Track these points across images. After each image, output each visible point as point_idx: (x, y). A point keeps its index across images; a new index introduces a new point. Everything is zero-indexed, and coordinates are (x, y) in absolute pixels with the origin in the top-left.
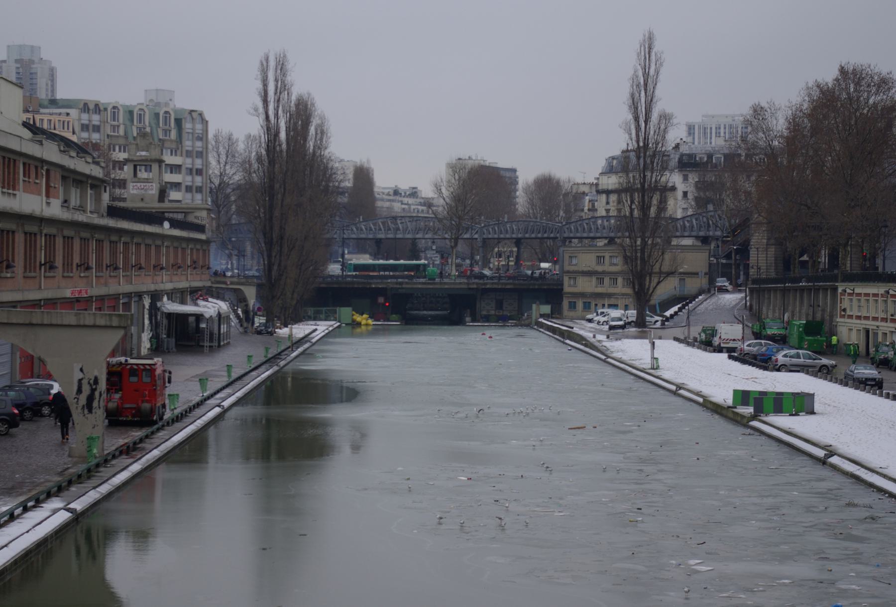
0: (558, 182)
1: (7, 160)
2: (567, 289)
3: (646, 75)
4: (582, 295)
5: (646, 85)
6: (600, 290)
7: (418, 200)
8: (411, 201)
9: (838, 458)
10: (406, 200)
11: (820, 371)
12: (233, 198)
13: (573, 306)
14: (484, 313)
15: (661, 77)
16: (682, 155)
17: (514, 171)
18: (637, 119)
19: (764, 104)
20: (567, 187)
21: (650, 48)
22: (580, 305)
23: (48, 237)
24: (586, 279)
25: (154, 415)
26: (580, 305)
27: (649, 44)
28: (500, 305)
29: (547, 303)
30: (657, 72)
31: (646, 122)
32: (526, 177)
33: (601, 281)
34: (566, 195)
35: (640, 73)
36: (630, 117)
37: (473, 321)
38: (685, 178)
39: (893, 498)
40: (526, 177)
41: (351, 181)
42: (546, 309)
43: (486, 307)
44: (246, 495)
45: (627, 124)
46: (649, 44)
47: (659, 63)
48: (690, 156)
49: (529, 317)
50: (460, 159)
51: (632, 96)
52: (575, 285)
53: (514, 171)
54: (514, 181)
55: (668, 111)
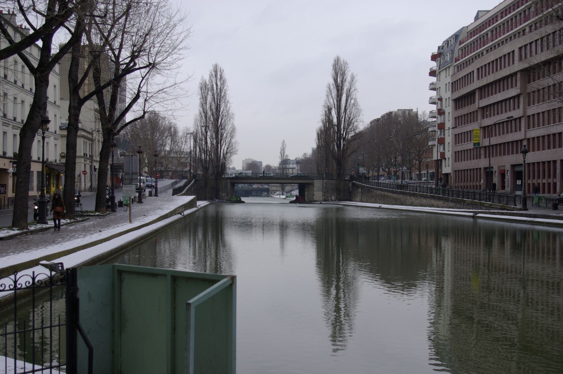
1: (85, 143)
2: (270, 189)
3: (283, 148)
4: (273, 190)
6: (277, 189)
8: (233, 171)
9: (274, 187)
10: (232, 170)
12: (310, 166)
15: (286, 148)
17: (261, 162)
18: (282, 156)
20: (273, 168)
22: (273, 193)
23: (457, 153)
26: (273, 193)
27: (284, 142)
28: (256, 193)
32: (264, 165)
33: (277, 187)
36: (280, 155)
38: (298, 166)
39: (88, 41)
40: (264, 165)
41: (35, 138)
43: (254, 193)
46: (284, 142)
53: (261, 162)
54: (261, 165)
55: (287, 154)
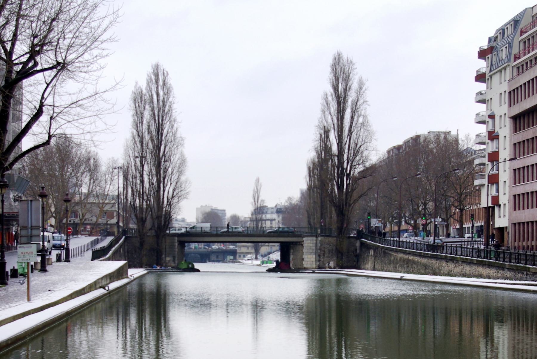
0: (238, 217)
2: (238, 251)
3: (257, 189)
4: (242, 253)
5: (257, 192)
6: (248, 251)
7: (185, 223)
8: (182, 223)
11: (33, 121)
13: (240, 256)
14: (213, 259)
16: (278, 209)
17: (224, 211)
19: (291, 197)
20: (242, 219)
21: (258, 182)
22: (242, 256)
24: (244, 248)
25: (162, 254)
26: (242, 256)
27: (258, 180)
28: (217, 257)
29: (232, 256)
30: (260, 188)
31: (257, 202)
32: (228, 215)
34: (242, 221)
35: (256, 189)
36: (253, 201)
37: (209, 261)
38: (279, 216)
40: (228, 215)
42: (232, 257)
43: (213, 257)
44: (347, 58)
45: (252, 202)
46: (258, 180)
47: (261, 186)
48: (280, 209)
49: (227, 260)
50: (202, 206)
51: (254, 194)
52: (240, 250)
53: (224, 211)
55: (264, 199)
